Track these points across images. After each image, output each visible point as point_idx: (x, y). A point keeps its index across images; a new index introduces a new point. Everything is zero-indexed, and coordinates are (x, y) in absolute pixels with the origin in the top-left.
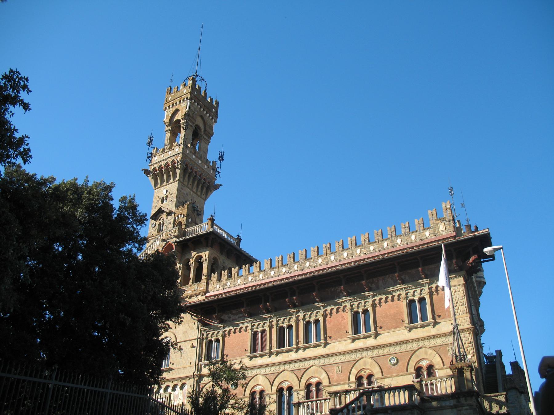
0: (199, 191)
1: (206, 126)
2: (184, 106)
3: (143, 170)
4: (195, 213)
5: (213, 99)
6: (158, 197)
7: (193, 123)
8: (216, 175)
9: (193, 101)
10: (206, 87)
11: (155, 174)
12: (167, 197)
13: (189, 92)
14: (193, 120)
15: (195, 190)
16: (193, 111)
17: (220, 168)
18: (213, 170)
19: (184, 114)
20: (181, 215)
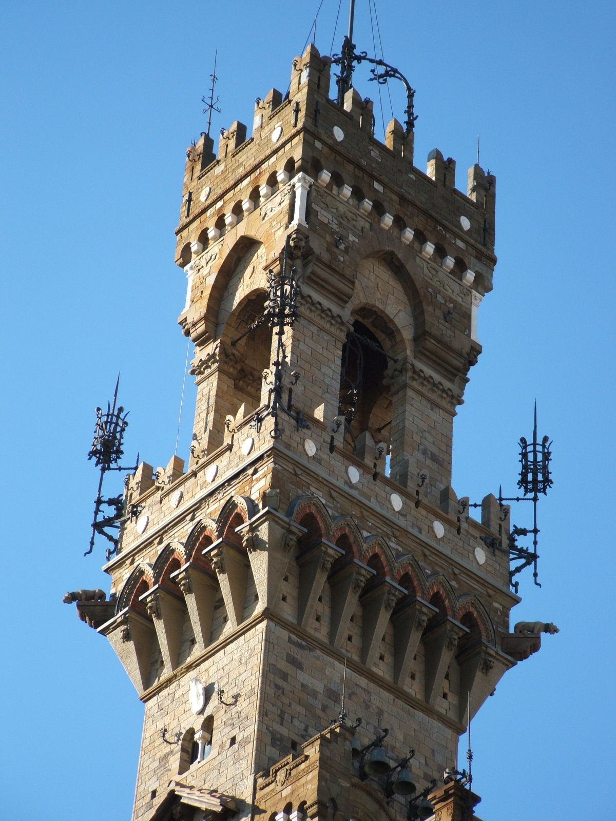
0: (413, 677)
1: (422, 312)
2: (277, 210)
3: (72, 598)
4: (396, 806)
5: (451, 162)
6: (161, 740)
7: (342, 298)
8: (512, 574)
9: (326, 176)
10: (410, 106)
11: (139, 608)
12: (208, 725)
13: (294, 131)
14: (335, 280)
15: (382, 670)
16: (332, 233)
17: (535, 531)
18: (492, 544)
19: (277, 255)
20: (288, 809)
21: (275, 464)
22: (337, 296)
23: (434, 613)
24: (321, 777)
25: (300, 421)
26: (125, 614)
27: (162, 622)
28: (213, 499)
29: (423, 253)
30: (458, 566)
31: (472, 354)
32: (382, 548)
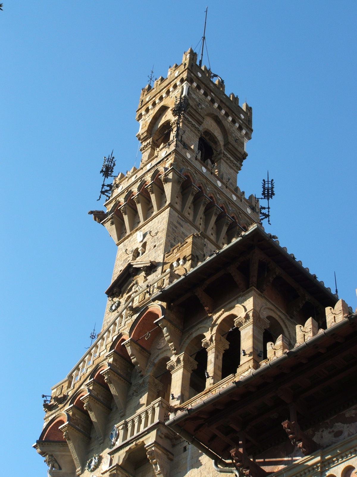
3: (91, 213)
12: (144, 245)
16: (197, 102)
17: (269, 208)
21: (176, 155)
22: (197, 121)
23: (233, 221)
24: (192, 248)
25: (185, 146)
26: (112, 215)
27: (127, 216)
28: (149, 173)
29: (228, 120)
30: (241, 210)
31: (244, 156)
32: (214, 195)
